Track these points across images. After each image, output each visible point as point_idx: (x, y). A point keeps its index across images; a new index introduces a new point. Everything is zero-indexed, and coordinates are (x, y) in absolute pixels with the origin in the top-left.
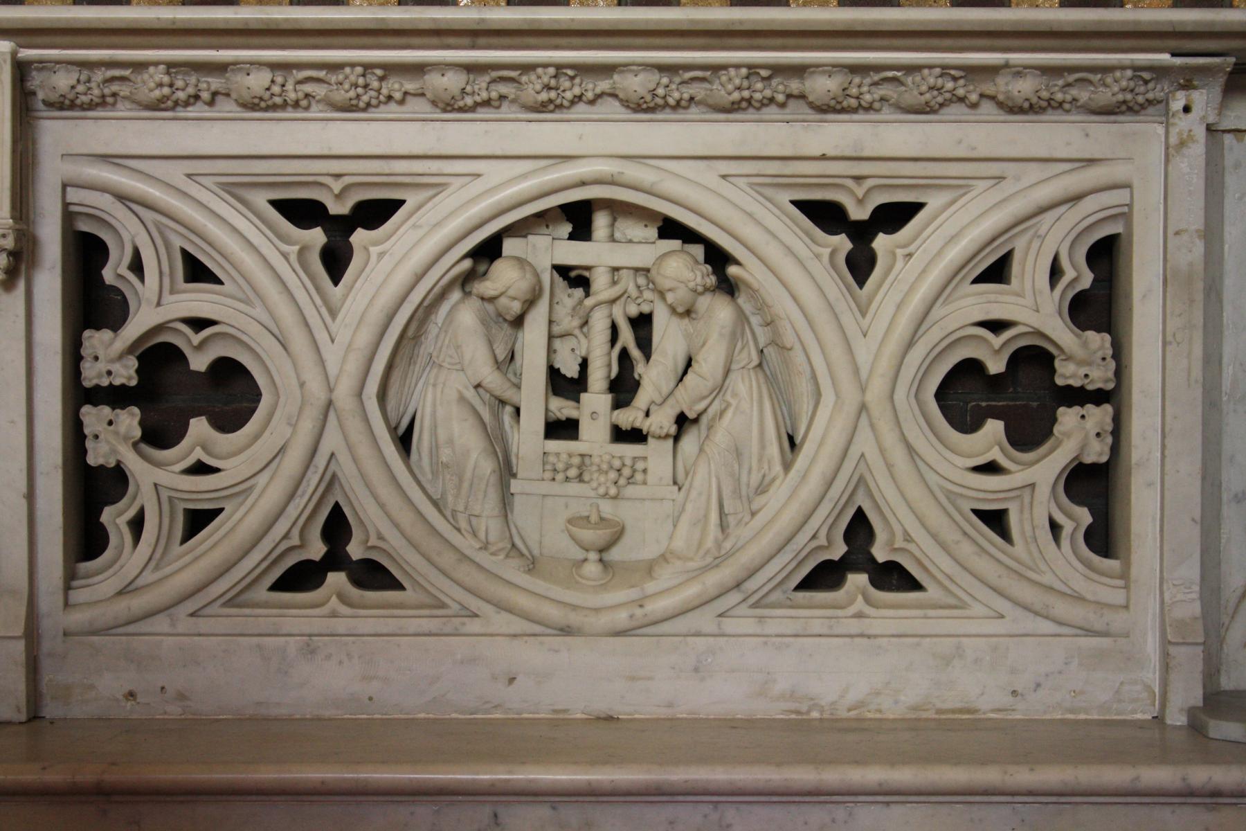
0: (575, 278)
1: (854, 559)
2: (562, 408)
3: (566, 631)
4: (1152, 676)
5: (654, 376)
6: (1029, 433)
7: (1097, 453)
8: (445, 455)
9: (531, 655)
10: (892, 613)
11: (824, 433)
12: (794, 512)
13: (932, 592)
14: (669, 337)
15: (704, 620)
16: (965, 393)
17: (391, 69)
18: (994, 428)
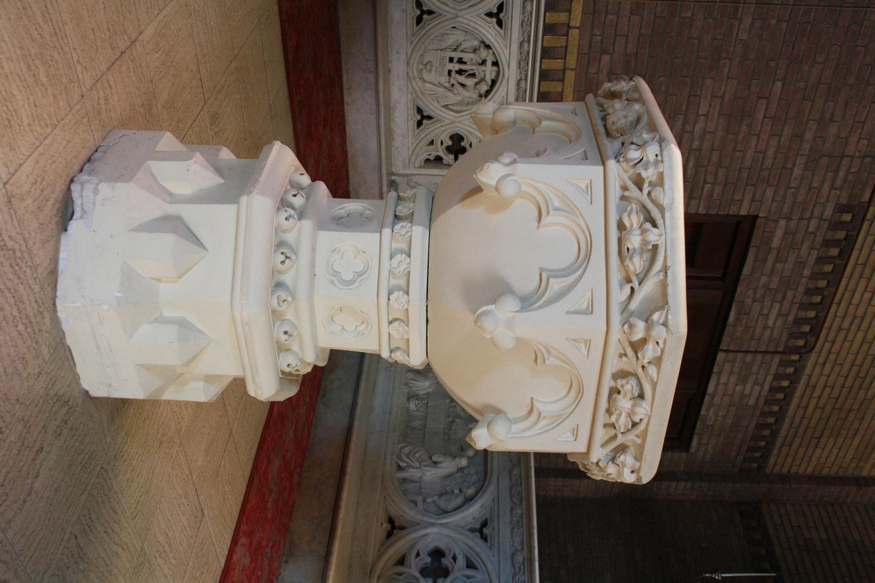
0: (484, 62)
1: (423, 118)
2: (455, 60)
3: (408, 63)
4: (401, 172)
5: (462, 79)
6: (449, 149)
7: (445, 162)
8: (446, 37)
9: (403, 57)
10: (412, 124)
11: (450, 116)
12: (432, 107)
13: (417, 131)
14: (470, 82)
15: (410, 90)
16: (457, 138)
17: (529, 36)
18: (450, 143)
